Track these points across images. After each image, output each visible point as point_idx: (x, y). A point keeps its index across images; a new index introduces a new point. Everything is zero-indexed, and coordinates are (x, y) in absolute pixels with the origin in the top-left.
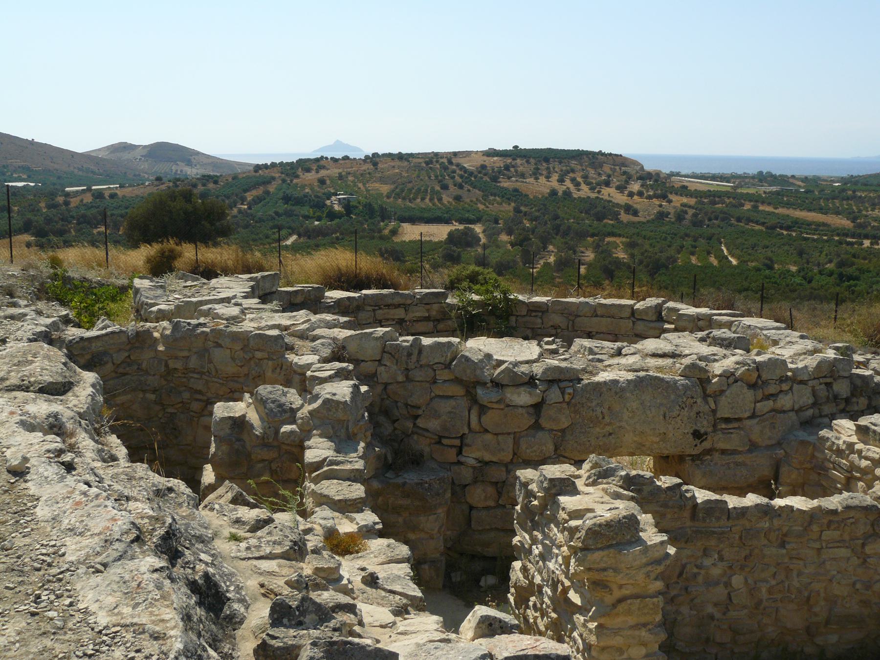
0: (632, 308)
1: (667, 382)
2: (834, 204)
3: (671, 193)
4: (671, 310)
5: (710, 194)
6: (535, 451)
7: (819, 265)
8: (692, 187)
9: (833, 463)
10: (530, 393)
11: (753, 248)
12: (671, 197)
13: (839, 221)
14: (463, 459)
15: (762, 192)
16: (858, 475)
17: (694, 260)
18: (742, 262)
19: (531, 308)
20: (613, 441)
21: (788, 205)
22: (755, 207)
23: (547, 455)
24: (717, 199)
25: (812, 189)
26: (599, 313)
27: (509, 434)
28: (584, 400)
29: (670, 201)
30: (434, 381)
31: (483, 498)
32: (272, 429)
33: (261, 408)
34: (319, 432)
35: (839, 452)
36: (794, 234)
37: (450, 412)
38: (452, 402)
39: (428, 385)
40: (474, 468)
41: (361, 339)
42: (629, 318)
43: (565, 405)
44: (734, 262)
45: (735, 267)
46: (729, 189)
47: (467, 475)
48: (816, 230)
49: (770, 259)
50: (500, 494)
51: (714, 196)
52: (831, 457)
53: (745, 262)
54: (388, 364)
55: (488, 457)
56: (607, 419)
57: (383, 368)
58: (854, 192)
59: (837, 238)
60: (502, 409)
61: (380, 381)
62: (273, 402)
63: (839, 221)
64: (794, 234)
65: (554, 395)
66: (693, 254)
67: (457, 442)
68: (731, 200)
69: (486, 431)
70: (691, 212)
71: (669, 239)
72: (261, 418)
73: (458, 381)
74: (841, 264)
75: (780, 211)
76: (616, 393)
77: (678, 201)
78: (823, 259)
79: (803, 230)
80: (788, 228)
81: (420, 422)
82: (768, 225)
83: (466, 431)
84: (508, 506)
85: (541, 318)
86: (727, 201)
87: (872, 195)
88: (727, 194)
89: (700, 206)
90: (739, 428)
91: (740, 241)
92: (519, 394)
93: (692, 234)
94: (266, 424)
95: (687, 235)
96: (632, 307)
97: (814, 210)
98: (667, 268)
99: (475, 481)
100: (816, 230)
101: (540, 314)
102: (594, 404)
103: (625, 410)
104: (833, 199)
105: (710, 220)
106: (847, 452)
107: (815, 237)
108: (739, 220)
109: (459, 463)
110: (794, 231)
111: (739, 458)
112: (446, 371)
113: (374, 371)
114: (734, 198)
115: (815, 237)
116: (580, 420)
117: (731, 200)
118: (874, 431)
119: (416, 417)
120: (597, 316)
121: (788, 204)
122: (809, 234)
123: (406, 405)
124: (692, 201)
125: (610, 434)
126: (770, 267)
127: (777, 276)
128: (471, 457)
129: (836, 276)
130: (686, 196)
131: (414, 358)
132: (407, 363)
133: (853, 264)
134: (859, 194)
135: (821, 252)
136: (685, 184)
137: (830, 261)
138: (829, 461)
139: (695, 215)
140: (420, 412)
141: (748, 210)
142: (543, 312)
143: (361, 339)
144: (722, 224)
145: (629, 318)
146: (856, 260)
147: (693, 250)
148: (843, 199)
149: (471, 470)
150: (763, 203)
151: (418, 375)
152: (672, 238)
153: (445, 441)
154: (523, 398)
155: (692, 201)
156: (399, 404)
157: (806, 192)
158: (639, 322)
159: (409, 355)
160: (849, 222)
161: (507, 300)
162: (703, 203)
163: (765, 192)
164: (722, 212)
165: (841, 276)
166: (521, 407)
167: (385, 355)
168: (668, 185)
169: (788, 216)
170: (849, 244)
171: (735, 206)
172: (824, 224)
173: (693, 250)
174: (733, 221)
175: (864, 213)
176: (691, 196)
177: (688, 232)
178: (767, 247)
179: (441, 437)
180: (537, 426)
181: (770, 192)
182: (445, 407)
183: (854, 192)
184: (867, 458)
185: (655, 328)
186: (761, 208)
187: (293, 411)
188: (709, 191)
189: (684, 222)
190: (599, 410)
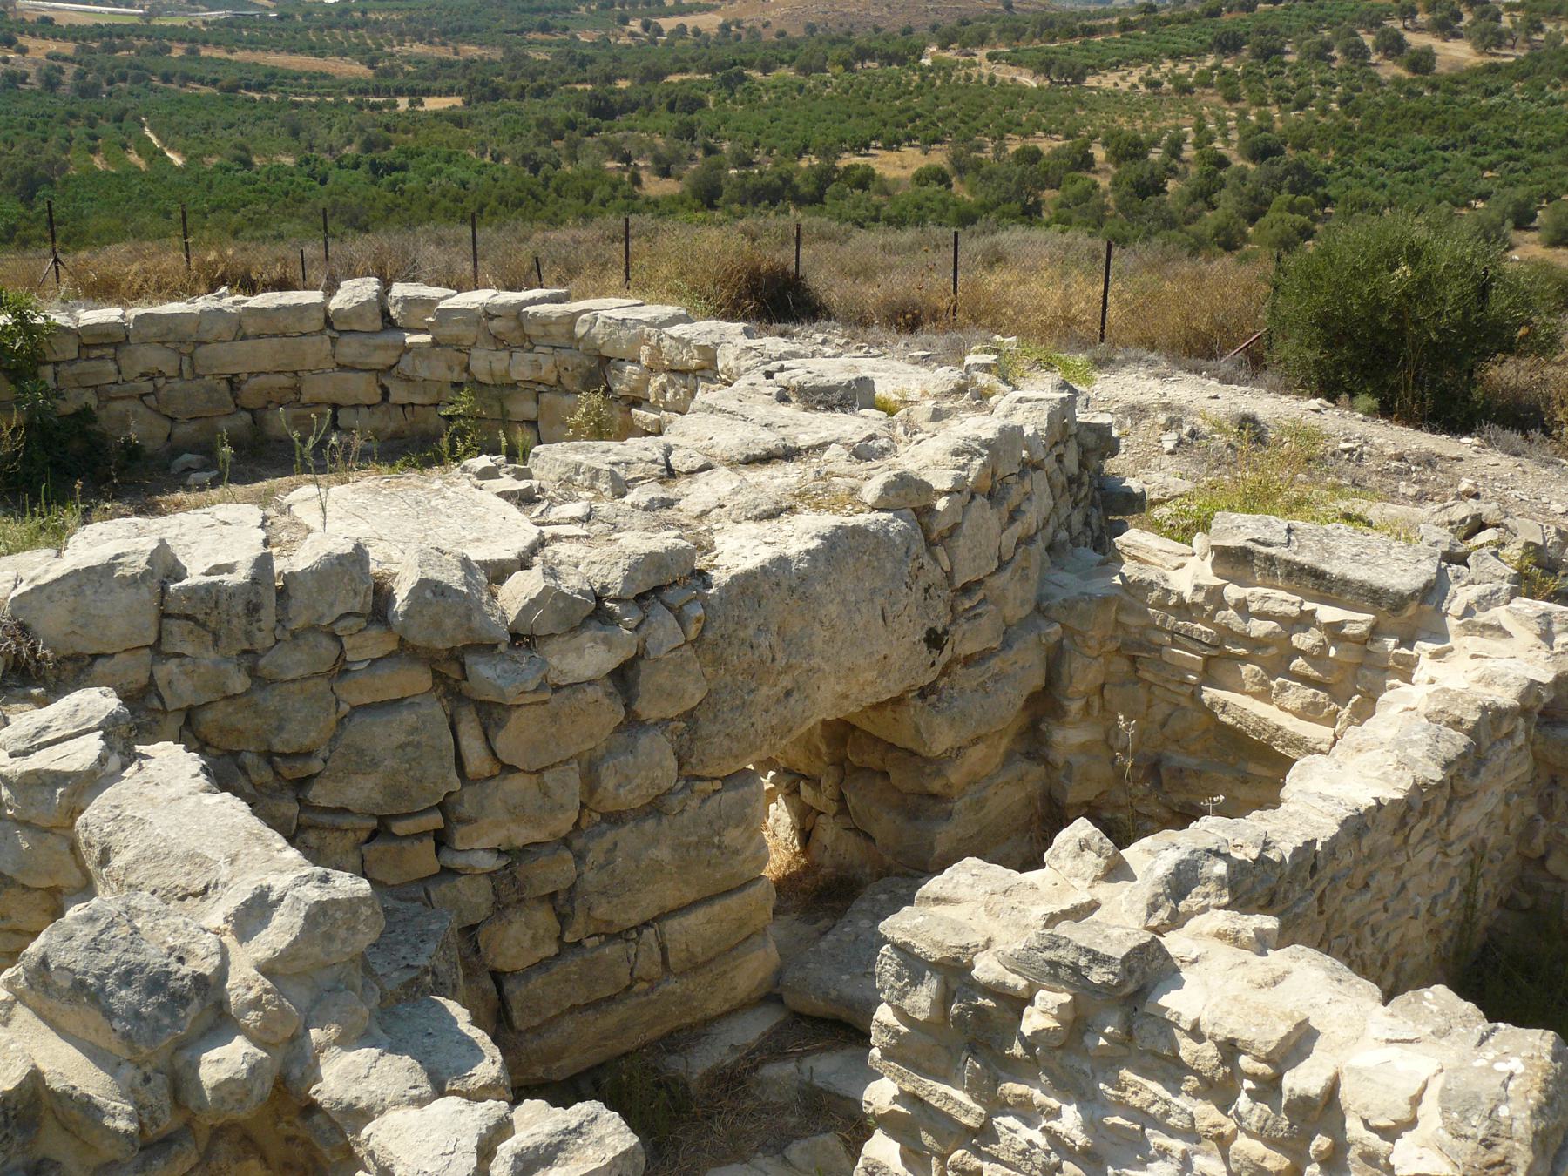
0: (326, 310)
1: (875, 534)
2: (333, 37)
3: (22, 33)
4: (408, 302)
5: (98, 32)
6: (638, 786)
7: (331, 149)
8: (62, 20)
9: (1173, 633)
10: (607, 642)
11: (206, 130)
12: (24, 41)
13: (346, 68)
14: (459, 861)
15: (200, 23)
16: (1242, 651)
17: (99, 162)
18: (192, 159)
19: (86, 340)
20: (799, 709)
21: (252, 44)
22: (193, 52)
23: (665, 786)
24: (117, 41)
25: (289, 11)
26: (250, 331)
27: (566, 762)
28: (731, 626)
29: (23, 51)
30: (341, 669)
31: (527, 943)
32: (158, 1080)
33: (85, 1018)
34: (333, 1031)
35: (1184, 609)
36: (274, 98)
37: (402, 747)
38: (408, 717)
39: (323, 685)
40: (490, 874)
41: (78, 591)
42: (321, 332)
43: (689, 652)
44: (178, 161)
45: (178, 169)
46: (135, 20)
47: (474, 896)
48: (310, 87)
49: (244, 148)
50: (563, 919)
51: (110, 35)
52: (1164, 621)
53: (197, 156)
54: (188, 649)
55: (523, 835)
56: (781, 661)
57: (172, 665)
58: (364, 13)
59: (350, 99)
60: (545, 702)
61: (172, 704)
62: (126, 979)
63: (346, 68)
64: (274, 98)
65: (664, 631)
66: (93, 150)
67: (435, 821)
68: (144, 41)
69: (509, 769)
70: (70, 70)
71: (39, 126)
72: (96, 1054)
73: (406, 651)
74: (369, 146)
75: (240, 55)
76: (792, 590)
77: (40, 48)
78: (334, 138)
79: (288, 89)
80: (260, 87)
81: (319, 794)
82: (224, 83)
83: (456, 784)
84: (589, 943)
85: (114, 360)
86: (138, 43)
87: (394, 17)
88: (133, 30)
89: (86, 57)
90: (983, 601)
91: (177, 119)
92: (580, 651)
93: (85, 112)
94: (128, 1072)
95: (73, 115)
96: (323, 307)
97: (300, 51)
98: (51, 183)
99: (500, 908)
100: (310, 87)
101: (112, 351)
102: (751, 631)
103: (817, 625)
104: (330, 28)
105: (111, 82)
106: (1209, 608)
107: (313, 99)
108: (167, 78)
109: (448, 872)
110: (274, 91)
111: (995, 664)
112: (374, 632)
113: (144, 680)
114: (149, 38)
115: (313, 99)
116: (728, 678)
117: (144, 41)
118: (1270, 559)
119: (303, 783)
120: (245, 337)
121: (252, 42)
122: (300, 95)
123: (269, 756)
124: (68, 48)
125: (788, 694)
126: (247, 164)
127: (262, 177)
128: (477, 850)
129: (366, 167)
130: (54, 37)
131: (268, 616)
132: (249, 635)
133: (387, 145)
134: (372, 16)
135: (330, 127)
136: (46, 14)
137: (350, 142)
138: (1161, 629)
139: (80, 76)
140: (315, 766)
141: (181, 58)
142: (117, 346)
143: (78, 591)
144: (137, 89)
145: (321, 332)
146: (392, 136)
147: (91, 143)
148: (348, 28)
149: (485, 883)
150: (205, 43)
151: (292, 662)
152: (46, 124)
153: (400, 828)
154: (590, 658)
155: (68, 48)
156: (248, 759)
157: (281, 18)
158: (346, 339)
159: (253, 609)
160: (364, 68)
161: (24, 326)
162: (91, 51)
163: (205, 23)
164: (133, 66)
165: (374, 167)
166: (590, 682)
167: (174, 626)
168: (11, 17)
169: (256, 64)
170: (374, 107)
171: (155, 53)
172: (324, 76)
173: (91, 143)
174: (156, 82)
175: (387, 49)
176: (64, 38)
177: (74, 108)
178: (232, 126)
179: (382, 820)
180: (632, 723)
181: (215, 22)
182: (384, 735)
183: (364, 13)
184: (1263, 616)
185: (386, 347)
186: (204, 53)
187: (210, 987)
188: (98, 26)
189: (61, 91)
190: (764, 641)
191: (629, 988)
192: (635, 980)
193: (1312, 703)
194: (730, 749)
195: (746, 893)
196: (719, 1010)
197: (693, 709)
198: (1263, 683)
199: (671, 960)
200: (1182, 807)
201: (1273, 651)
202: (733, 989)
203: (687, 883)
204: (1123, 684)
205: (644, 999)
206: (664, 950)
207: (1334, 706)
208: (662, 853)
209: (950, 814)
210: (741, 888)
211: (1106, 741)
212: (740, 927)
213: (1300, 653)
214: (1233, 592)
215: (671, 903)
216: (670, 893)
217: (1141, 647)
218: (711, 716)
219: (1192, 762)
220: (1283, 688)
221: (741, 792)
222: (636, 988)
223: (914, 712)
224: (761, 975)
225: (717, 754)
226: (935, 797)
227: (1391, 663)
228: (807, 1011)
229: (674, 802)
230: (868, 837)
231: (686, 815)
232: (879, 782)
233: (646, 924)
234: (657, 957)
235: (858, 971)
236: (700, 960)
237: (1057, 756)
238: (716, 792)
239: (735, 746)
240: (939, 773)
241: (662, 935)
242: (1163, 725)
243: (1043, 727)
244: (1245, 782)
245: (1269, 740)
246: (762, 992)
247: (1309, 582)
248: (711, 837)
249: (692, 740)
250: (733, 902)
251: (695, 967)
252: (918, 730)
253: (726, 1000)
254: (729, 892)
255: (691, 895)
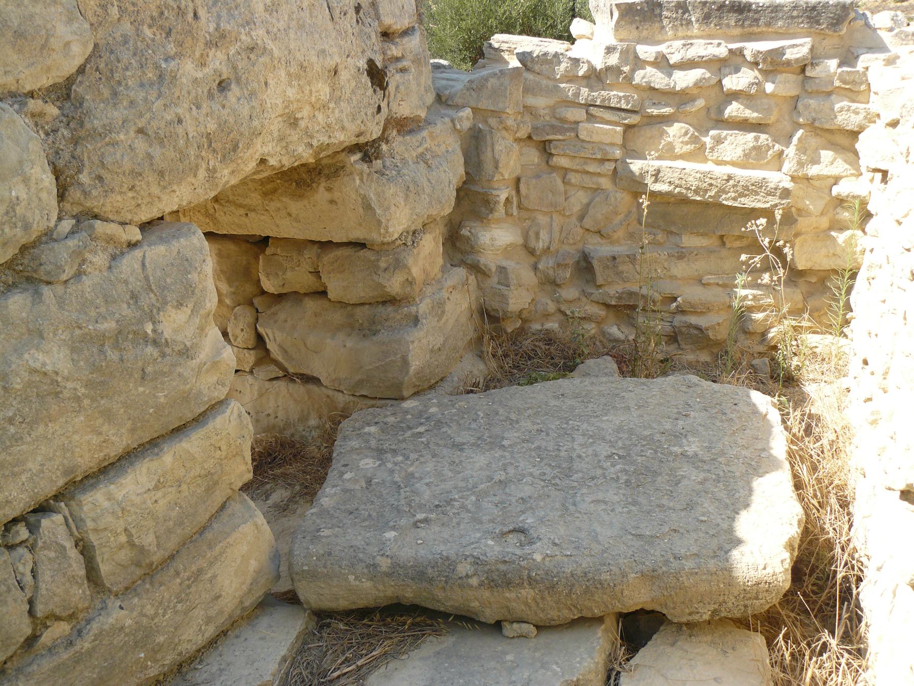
16: (667, 110)
23: (39, 225)
35: (595, 77)
52: (577, 94)
125: (223, 86)
138: (575, 104)
191: (31, 641)
192: (39, 623)
193: (754, 148)
194: (150, 157)
195: (211, 425)
196: (200, 640)
197: (70, 81)
198: (695, 140)
199: (104, 569)
200: (620, 298)
201: (700, 103)
202: (218, 597)
203: (108, 415)
204: (538, 177)
205: (65, 655)
206: (86, 550)
207: (777, 147)
208: (54, 357)
209: (416, 320)
210: (199, 420)
211: (526, 246)
212: (209, 490)
213: (735, 95)
214: (646, 51)
215: (86, 461)
216: (81, 439)
217: (554, 129)
218: (106, 92)
219: (620, 249)
220: (719, 141)
221: (175, 245)
222: (47, 638)
223: (358, 181)
224: (253, 565)
225: (127, 165)
226: (391, 301)
227: (837, 83)
228: (343, 604)
229: (61, 254)
230: (309, 379)
231: (87, 282)
232: (311, 305)
233: (43, 509)
234: (78, 568)
235: (403, 522)
236: (156, 558)
237: (489, 260)
238: (132, 245)
239: (156, 151)
240: (398, 265)
241: (79, 521)
242: (581, 218)
243: (465, 232)
244: (681, 257)
245: (718, 195)
246: (259, 593)
247: (732, 19)
248: (140, 322)
249: (76, 141)
250: (192, 444)
251: (148, 571)
252: (368, 207)
253: (209, 620)
254: (179, 430)
255: (120, 440)
